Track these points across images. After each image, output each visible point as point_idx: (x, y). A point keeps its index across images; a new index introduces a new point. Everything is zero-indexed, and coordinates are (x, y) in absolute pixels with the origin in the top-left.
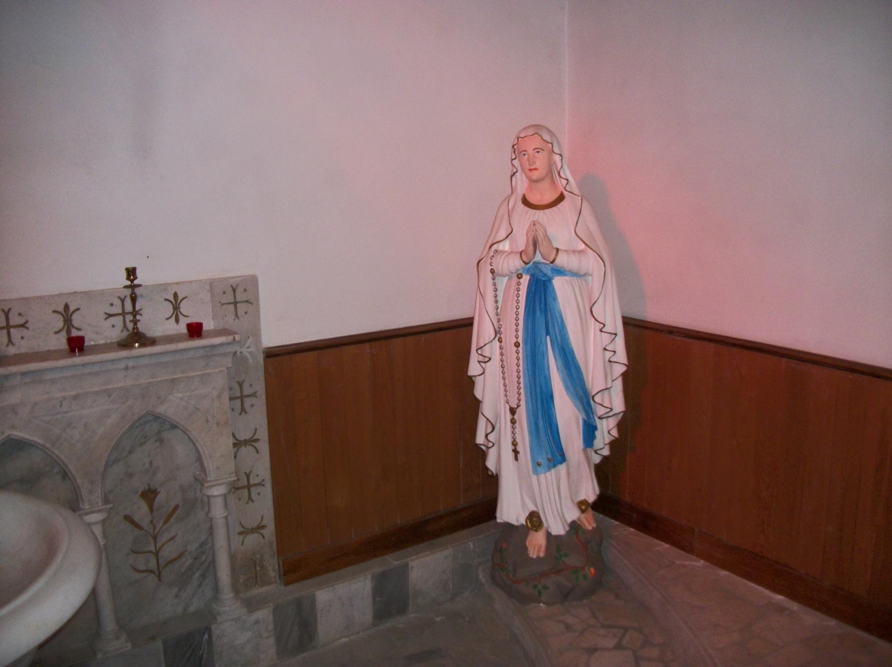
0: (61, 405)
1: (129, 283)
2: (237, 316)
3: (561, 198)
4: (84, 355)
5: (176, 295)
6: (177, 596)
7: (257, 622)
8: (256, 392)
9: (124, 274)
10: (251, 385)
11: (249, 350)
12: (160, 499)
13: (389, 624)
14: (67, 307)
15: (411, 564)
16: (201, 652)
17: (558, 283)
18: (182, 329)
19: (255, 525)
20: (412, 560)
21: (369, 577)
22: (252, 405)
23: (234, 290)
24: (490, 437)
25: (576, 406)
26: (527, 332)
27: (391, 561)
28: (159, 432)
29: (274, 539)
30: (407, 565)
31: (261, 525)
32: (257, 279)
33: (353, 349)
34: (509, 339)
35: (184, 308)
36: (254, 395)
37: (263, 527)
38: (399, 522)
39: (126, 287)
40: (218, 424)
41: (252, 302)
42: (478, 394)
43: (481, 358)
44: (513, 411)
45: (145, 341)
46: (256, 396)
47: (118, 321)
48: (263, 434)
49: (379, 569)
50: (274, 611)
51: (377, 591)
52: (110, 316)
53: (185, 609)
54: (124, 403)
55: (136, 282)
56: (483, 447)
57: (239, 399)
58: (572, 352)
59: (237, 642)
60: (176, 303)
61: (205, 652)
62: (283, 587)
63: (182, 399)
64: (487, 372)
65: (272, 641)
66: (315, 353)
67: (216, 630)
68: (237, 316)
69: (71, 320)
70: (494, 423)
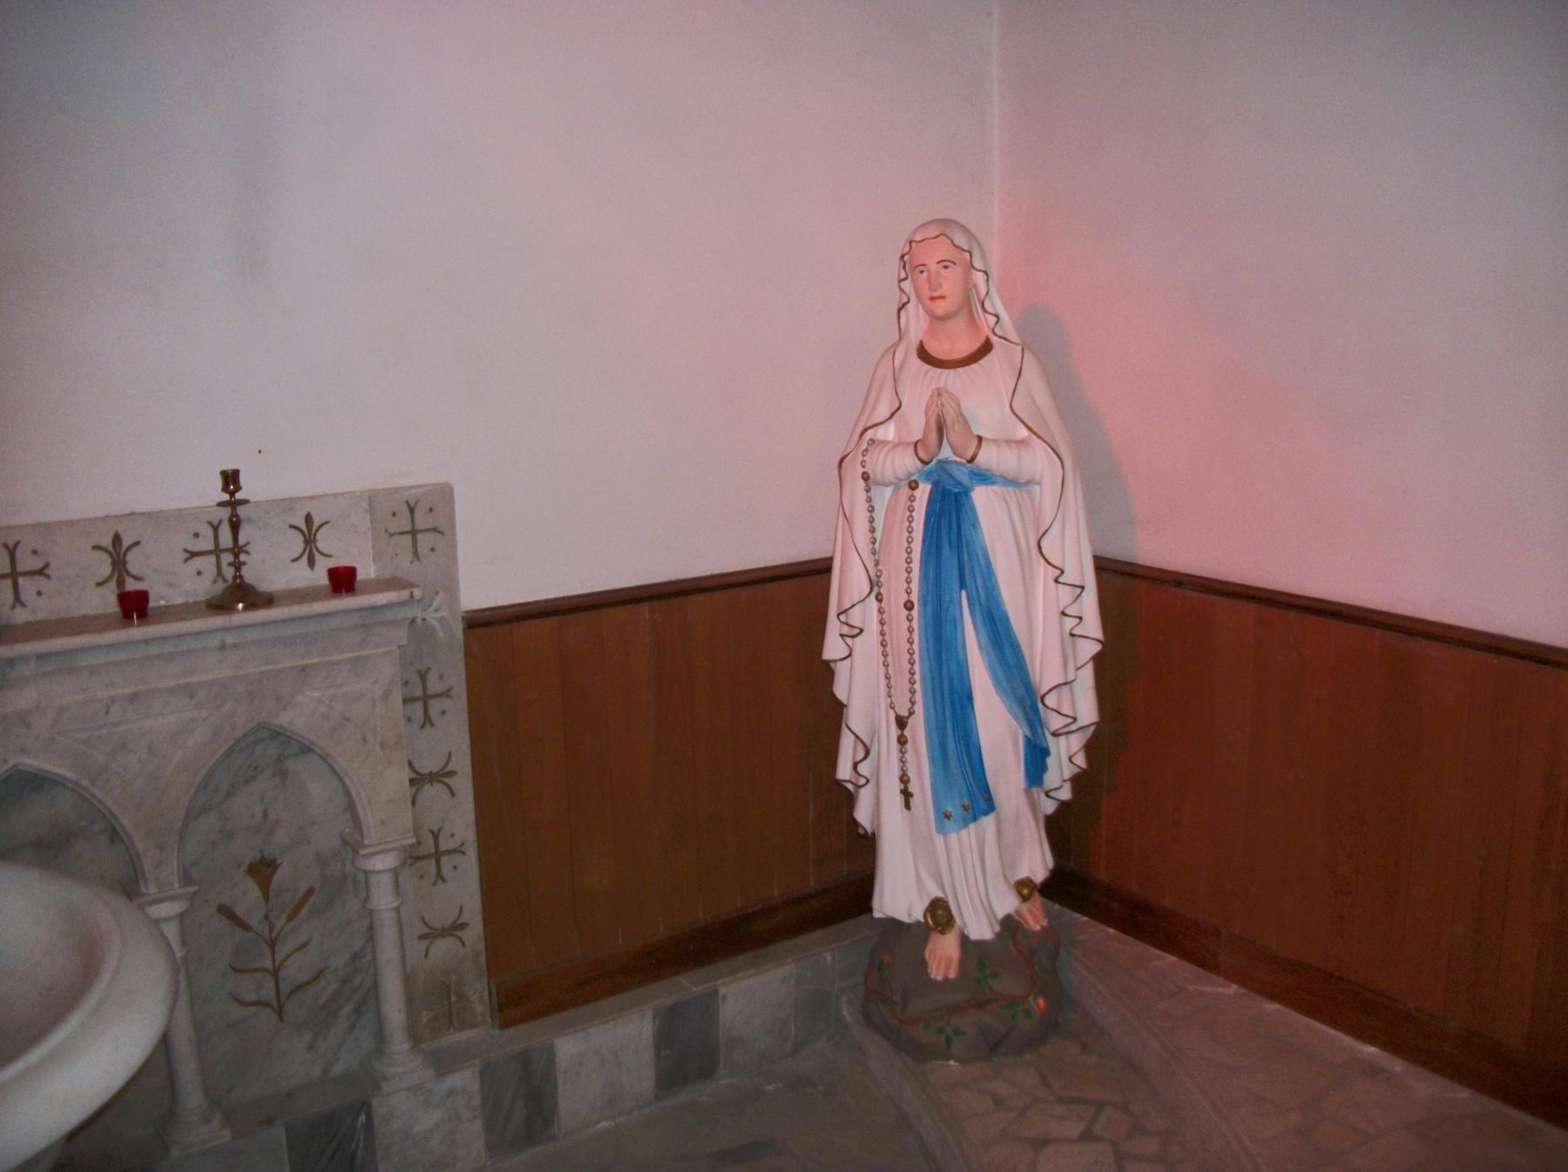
0: (107, 712)
1: (226, 497)
2: (416, 554)
3: (986, 348)
4: (147, 624)
5: (309, 519)
6: (311, 1048)
7: (451, 1093)
8: (450, 689)
9: (218, 482)
10: (441, 677)
11: (439, 615)
12: (281, 876)
13: (683, 1096)
14: (117, 539)
15: (722, 991)
16: (353, 1146)
17: (981, 496)
18: (320, 577)
19: (449, 922)
20: (724, 984)
21: (649, 1014)
22: (444, 712)
23: (412, 510)
24: (862, 768)
25: (1013, 714)
26: (927, 584)
27: (687, 985)
28: (280, 759)
29: (481, 946)
30: (716, 992)
31: (459, 922)
32: (452, 490)
33: (621, 612)
34: (896, 596)
35: (324, 541)
36: (446, 694)
37: (463, 926)
38: (701, 917)
39: (222, 504)
40: (383, 745)
41: (443, 530)
42: (840, 692)
43: (846, 630)
44: (901, 723)
45: (255, 599)
46: (450, 697)
47: (207, 563)
48: (463, 763)
49: (666, 1000)
50: (482, 1073)
51: (663, 1038)
52: (193, 555)
53: (325, 1071)
54: (218, 708)
55: (239, 496)
56: (850, 786)
57: (421, 701)
58: (1006, 619)
59: (417, 1129)
60: (309, 533)
61: (361, 1146)
62: (497, 1032)
63: (319, 701)
64: (856, 654)
65: (478, 1126)
66: (555, 620)
67: (379, 1107)
68: (416, 554)
69: (124, 563)
70: (868, 744)
